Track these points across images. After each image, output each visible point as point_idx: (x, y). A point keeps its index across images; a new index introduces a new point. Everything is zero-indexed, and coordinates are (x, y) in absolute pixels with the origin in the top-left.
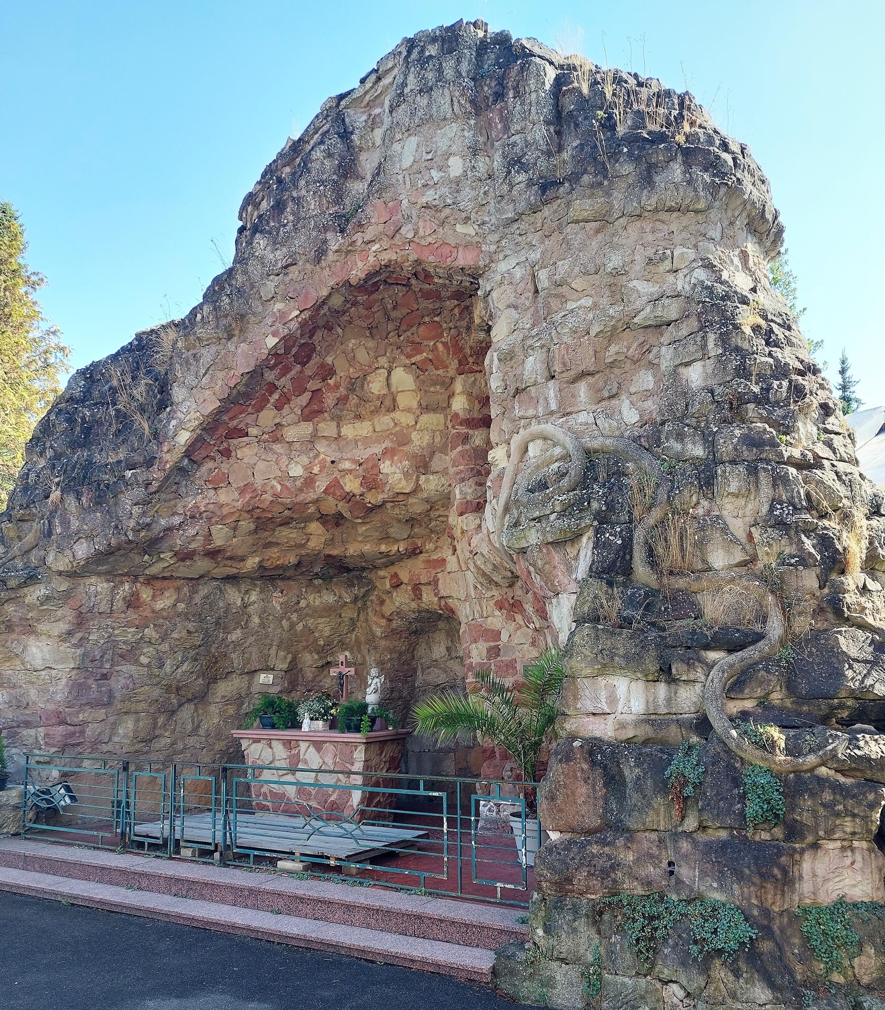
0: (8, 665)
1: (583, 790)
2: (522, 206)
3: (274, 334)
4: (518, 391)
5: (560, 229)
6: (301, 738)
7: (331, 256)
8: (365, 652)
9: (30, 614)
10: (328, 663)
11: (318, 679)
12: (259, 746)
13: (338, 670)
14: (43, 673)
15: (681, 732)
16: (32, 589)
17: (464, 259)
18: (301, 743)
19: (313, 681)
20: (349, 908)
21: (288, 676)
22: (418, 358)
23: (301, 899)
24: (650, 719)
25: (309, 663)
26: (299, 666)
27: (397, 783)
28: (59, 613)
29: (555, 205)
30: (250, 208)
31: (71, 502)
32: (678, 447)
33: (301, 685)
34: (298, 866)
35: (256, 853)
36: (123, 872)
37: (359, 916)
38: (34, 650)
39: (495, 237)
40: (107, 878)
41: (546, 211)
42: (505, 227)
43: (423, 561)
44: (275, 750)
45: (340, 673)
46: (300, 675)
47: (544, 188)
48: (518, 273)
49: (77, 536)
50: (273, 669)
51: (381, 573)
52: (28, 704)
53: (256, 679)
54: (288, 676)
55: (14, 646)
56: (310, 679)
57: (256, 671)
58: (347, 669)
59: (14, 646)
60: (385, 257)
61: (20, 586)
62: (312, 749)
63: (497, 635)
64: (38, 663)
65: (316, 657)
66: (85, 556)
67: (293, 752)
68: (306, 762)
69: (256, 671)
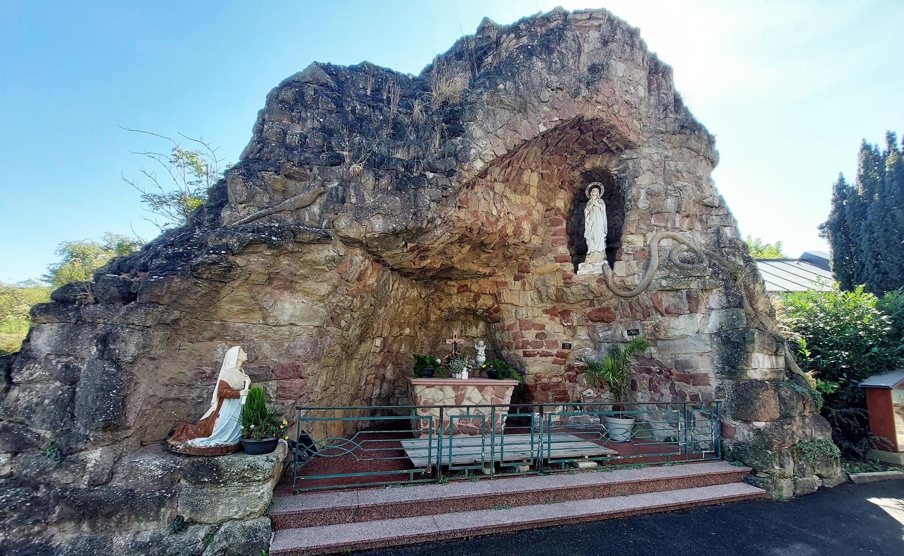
0: (242, 317)
1: (773, 402)
2: (670, 129)
3: (545, 125)
4: (658, 213)
5: (681, 147)
7: (580, 98)
9: (301, 271)
13: (452, 341)
14: (284, 328)
16: (320, 247)
17: (632, 137)
20: (668, 480)
22: (544, 172)
23: (640, 483)
24: (773, 370)
27: (390, 413)
28: (328, 275)
29: (682, 136)
30: (513, 35)
31: (369, 180)
32: (733, 259)
34: (582, 465)
35: (470, 468)
36: (487, 497)
37: (674, 483)
38: (287, 305)
39: (648, 135)
40: (470, 506)
41: (678, 137)
42: (656, 133)
43: (492, 281)
47: (682, 127)
48: (656, 157)
49: (375, 210)
51: (452, 283)
52: (257, 358)
55: (265, 299)
59: (265, 299)
60: (602, 115)
61: (311, 243)
62: (476, 390)
63: (543, 327)
64: (285, 319)
66: (381, 230)
68: (469, 399)
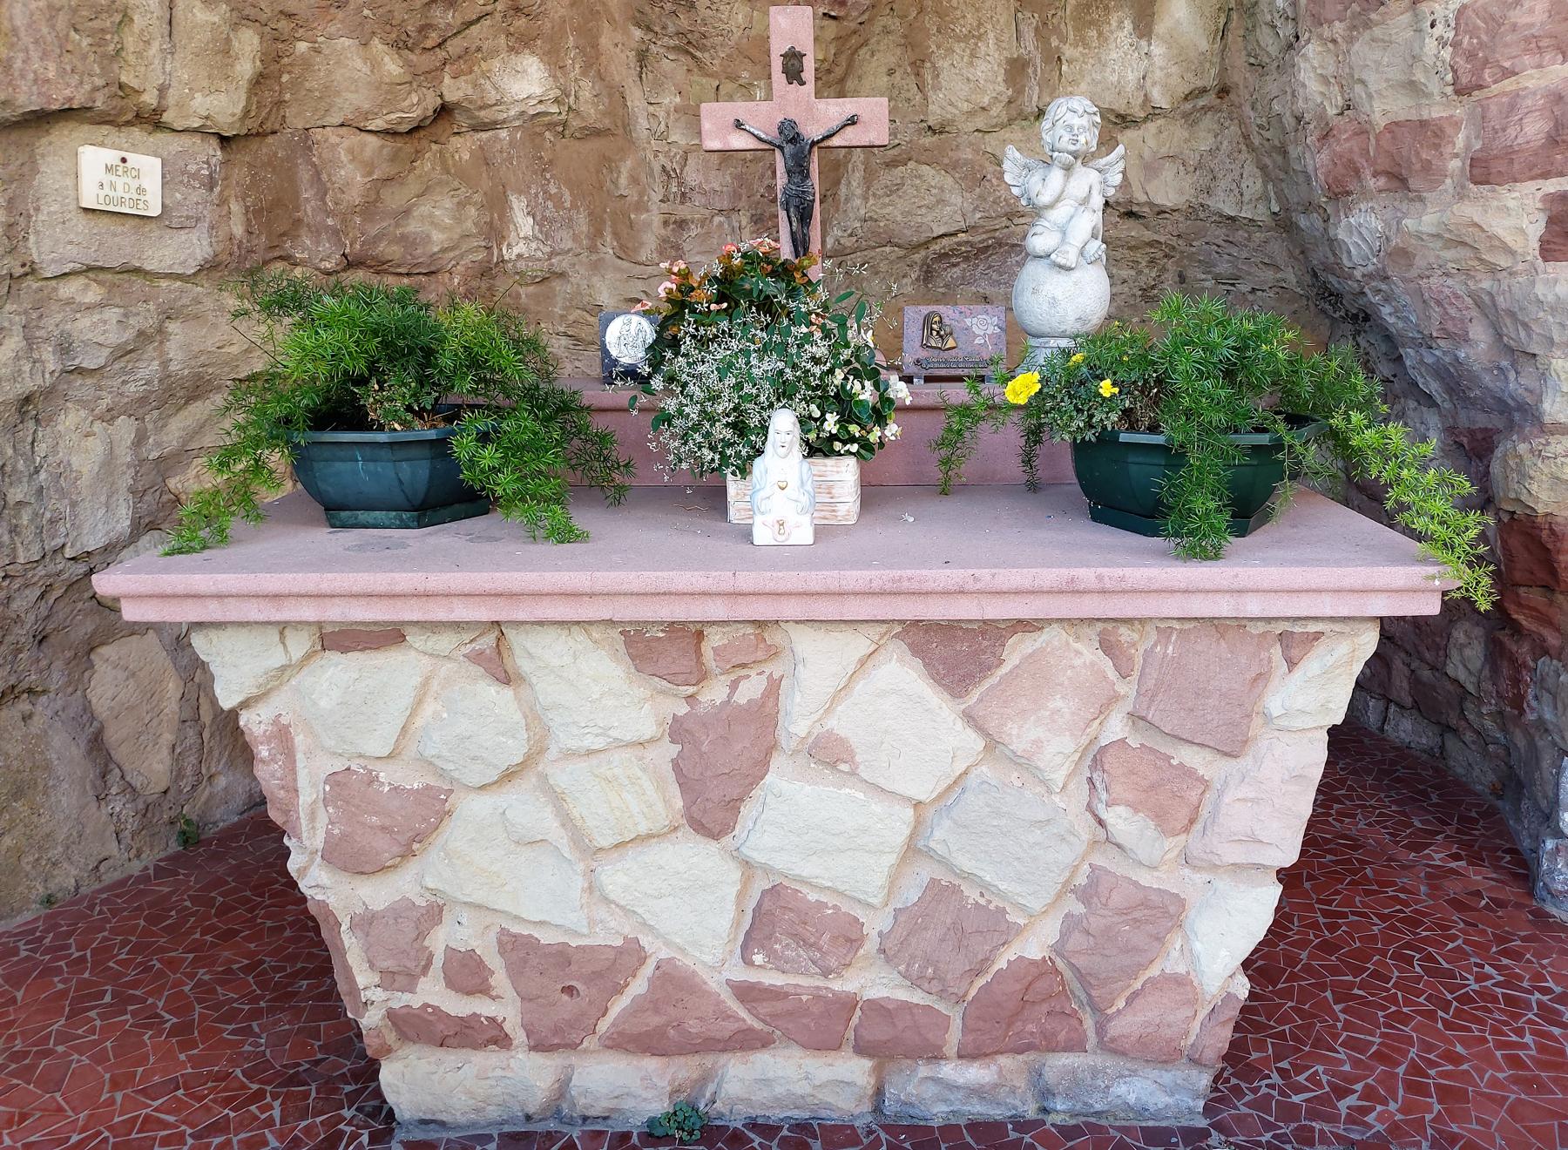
6: (790, 609)
8: (620, 64)
10: (444, 111)
11: (394, 198)
12: (396, 671)
13: (763, 116)
15: (1063, 336)
18: (806, 643)
19: (369, 208)
21: (240, 174)
25: (353, 100)
26: (296, 119)
33: (316, 232)
44: (546, 689)
45: (790, 135)
46: (305, 174)
50: (152, 120)
53: (50, 175)
54: (240, 174)
56: (354, 196)
57: (42, 119)
58: (834, 110)
65: (392, 66)
67: (714, 693)
69: (42, 119)
